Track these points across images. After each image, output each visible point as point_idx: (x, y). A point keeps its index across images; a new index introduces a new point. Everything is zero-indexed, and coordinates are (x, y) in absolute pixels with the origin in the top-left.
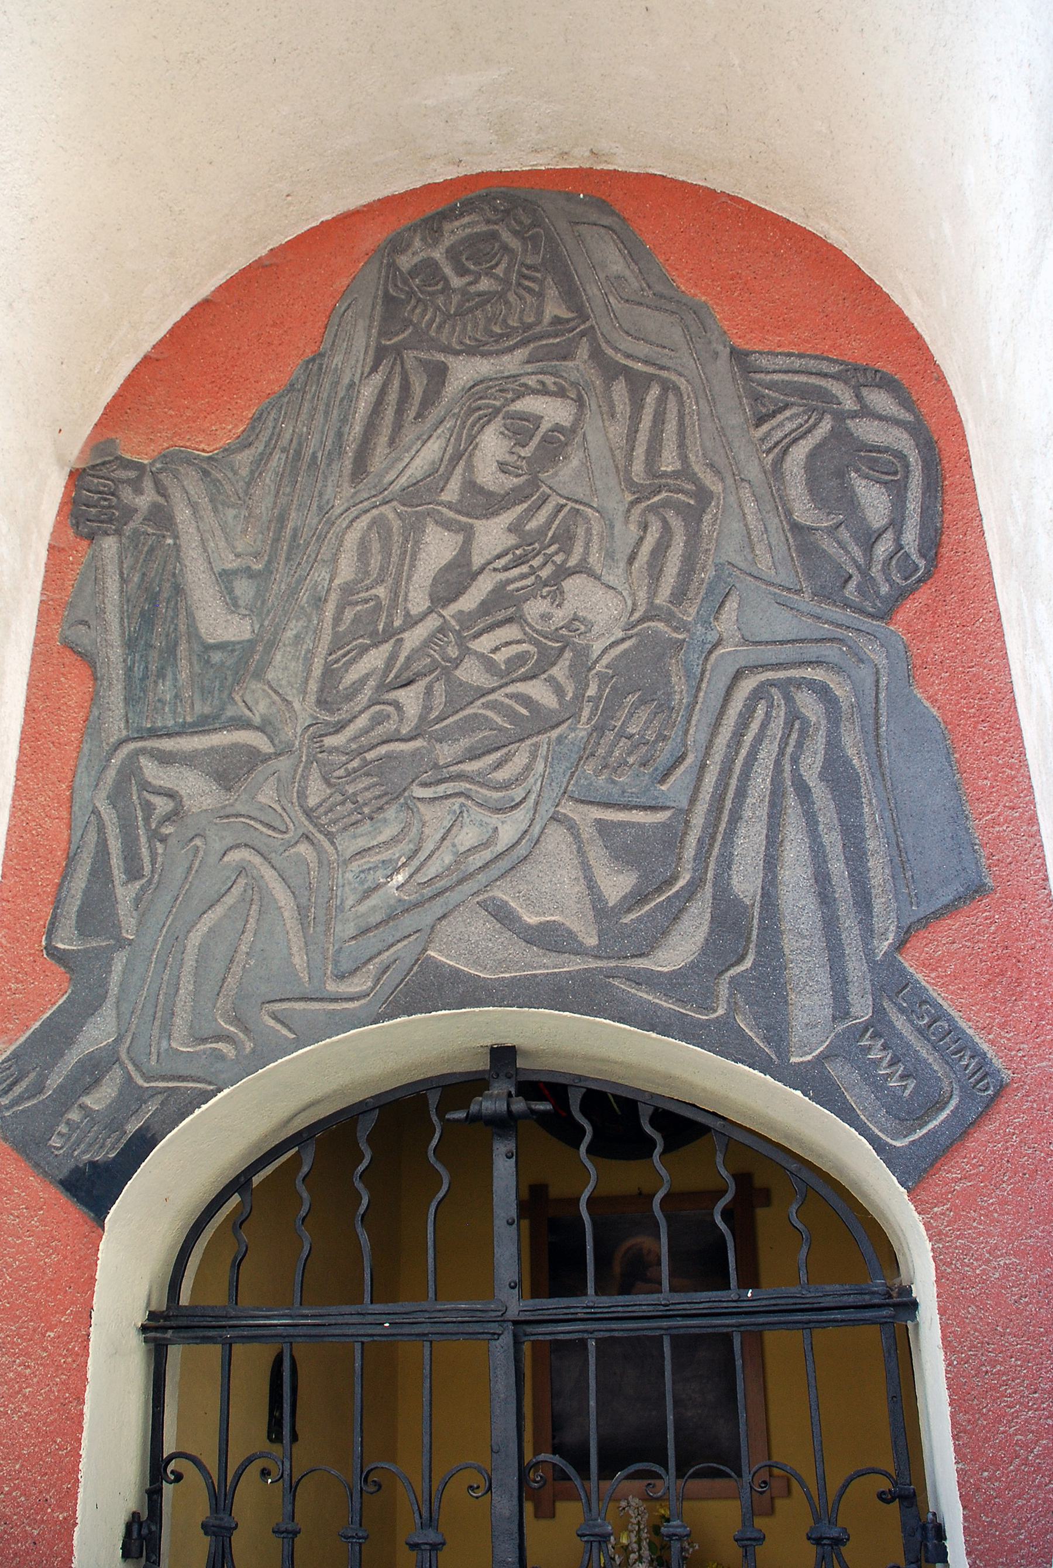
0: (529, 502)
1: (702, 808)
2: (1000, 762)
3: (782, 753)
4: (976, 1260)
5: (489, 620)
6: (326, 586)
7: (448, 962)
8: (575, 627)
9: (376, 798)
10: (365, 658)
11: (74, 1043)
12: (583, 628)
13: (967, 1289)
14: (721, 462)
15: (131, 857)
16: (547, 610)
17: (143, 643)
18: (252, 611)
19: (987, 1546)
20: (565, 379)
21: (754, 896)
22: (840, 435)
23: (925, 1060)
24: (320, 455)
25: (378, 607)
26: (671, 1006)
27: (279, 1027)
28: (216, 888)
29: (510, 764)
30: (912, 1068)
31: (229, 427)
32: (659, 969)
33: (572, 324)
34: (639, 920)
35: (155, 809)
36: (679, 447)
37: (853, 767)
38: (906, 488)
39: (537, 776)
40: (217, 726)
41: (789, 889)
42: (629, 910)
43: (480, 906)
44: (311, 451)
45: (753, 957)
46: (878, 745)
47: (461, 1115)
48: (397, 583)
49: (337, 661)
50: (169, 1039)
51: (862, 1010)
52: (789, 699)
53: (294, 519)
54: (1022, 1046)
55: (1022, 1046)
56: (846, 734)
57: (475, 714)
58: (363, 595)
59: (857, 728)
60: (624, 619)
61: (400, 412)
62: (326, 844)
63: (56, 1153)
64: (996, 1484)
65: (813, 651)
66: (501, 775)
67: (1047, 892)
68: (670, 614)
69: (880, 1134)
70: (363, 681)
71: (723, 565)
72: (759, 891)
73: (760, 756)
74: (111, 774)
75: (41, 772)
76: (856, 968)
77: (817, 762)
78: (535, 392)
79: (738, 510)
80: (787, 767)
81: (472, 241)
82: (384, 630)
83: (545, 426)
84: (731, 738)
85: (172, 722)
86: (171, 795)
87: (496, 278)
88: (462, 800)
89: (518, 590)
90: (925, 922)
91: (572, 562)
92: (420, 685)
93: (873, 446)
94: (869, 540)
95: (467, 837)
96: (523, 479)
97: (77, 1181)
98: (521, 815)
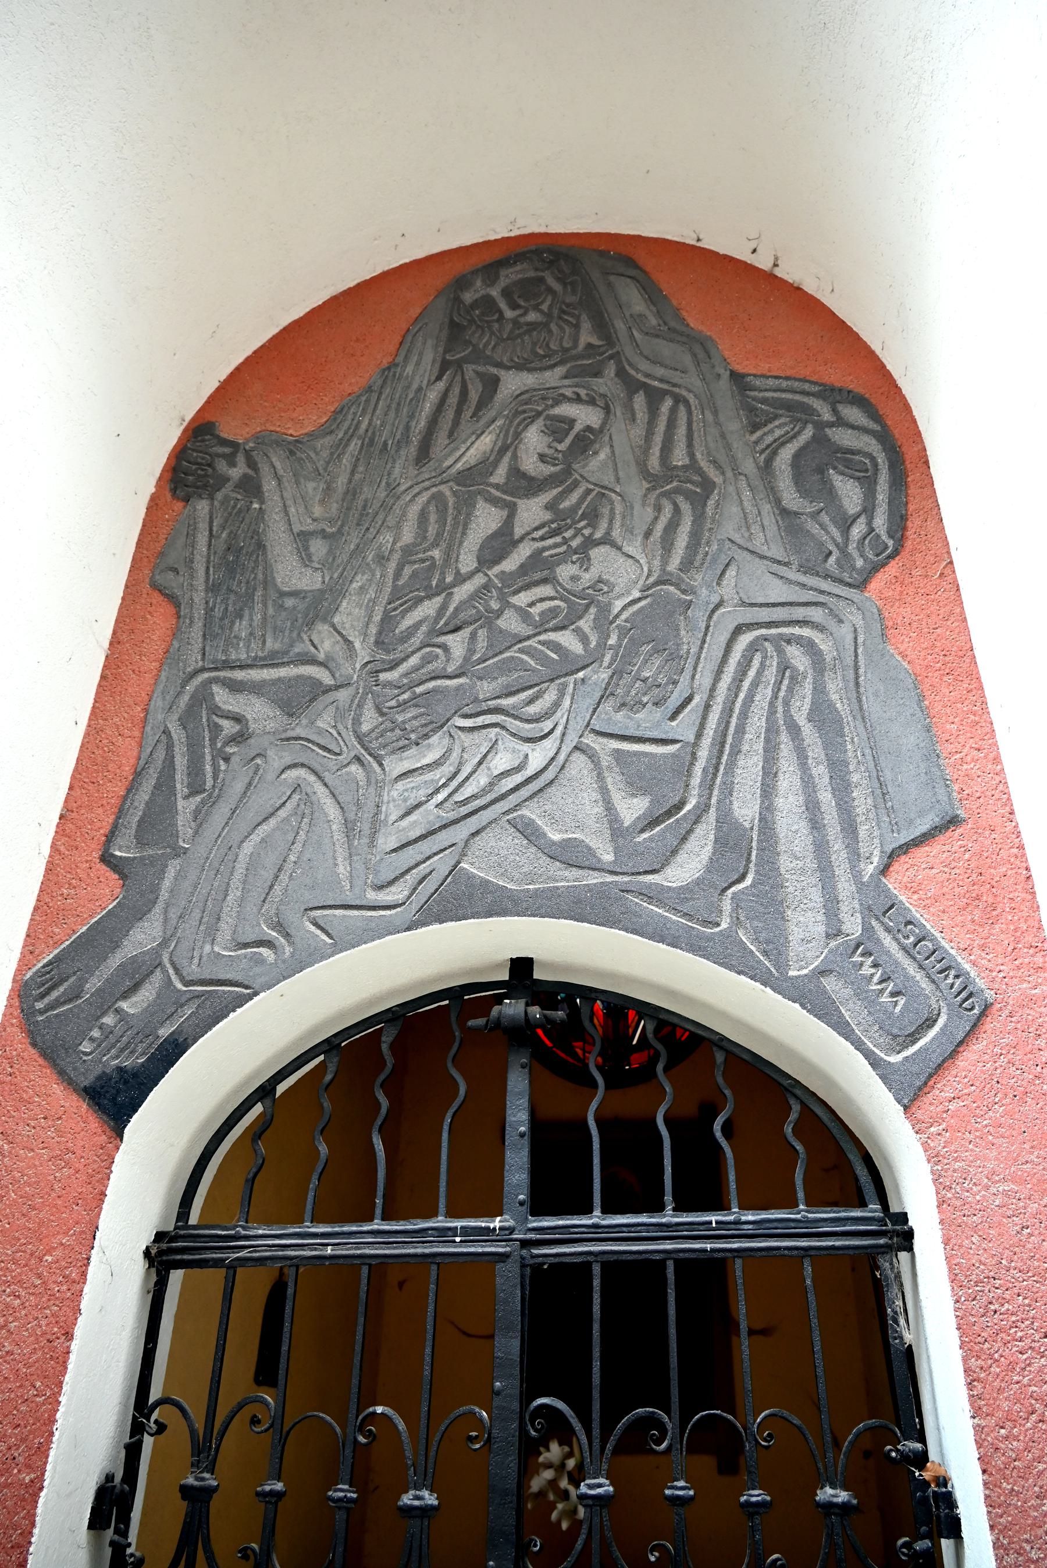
0: (563, 487)
1: (706, 741)
2: (965, 709)
3: (775, 696)
4: (975, 1184)
5: (527, 579)
6: (389, 547)
7: (479, 873)
8: (599, 588)
9: (422, 726)
10: (420, 608)
11: (118, 947)
12: (606, 589)
13: (968, 1216)
14: (722, 458)
15: (195, 770)
16: (576, 573)
17: (225, 588)
18: (323, 565)
19: (1010, 1519)
20: (595, 392)
21: (752, 821)
22: (820, 440)
23: (914, 977)
24: (390, 442)
25: (433, 565)
26: (680, 920)
27: (318, 932)
28: (272, 802)
29: (541, 700)
30: (901, 986)
31: (314, 418)
32: (670, 884)
33: (602, 350)
34: (651, 839)
35: (222, 731)
36: (687, 447)
37: (836, 710)
38: (875, 482)
39: (564, 711)
40: (285, 660)
41: (783, 815)
42: (642, 831)
43: (510, 823)
44: (383, 439)
45: (753, 875)
46: (858, 692)
47: (480, 1022)
48: (450, 547)
49: (395, 609)
50: (213, 944)
51: (853, 926)
52: (780, 652)
53: (367, 492)
54: (1002, 968)
55: (1002, 968)
56: (830, 682)
57: (512, 657)
58: (421, 556)
59: (839, 678)
60: (641, 582)
61: (459, 412)
62: (375, 765)
63: (85, 1058)
64: (1015, 1443)
65: (800, 613)
66: (532, 710)
67: (1014, 824)
68: (679, 579)
69: (874, 1049)
70: (417, 626)
71: (723, 540)
72: (757, 816)
73: (757, 698)
74: (185, 698)
75: (120, 696)
76: (845, 887)
77: (805, 705)
78: (569, 400)
79: (736, 497)
80: (780, 709)
81: (523, 283)
82: (437, 585)
83: (578, 427)
84: (732, 682)
85: (245, 656)
86: (237, 719)
87: (541, 312)
88: (497, 730)
89: (552, 556)
90: (905, 848)
91: (598, 535)
92: (466, 633)
93: (847, 449)
94: (846, 524)
95: (501, 762)
96: (558, 468)
97: (102, 1087)
98: (549, 746)
